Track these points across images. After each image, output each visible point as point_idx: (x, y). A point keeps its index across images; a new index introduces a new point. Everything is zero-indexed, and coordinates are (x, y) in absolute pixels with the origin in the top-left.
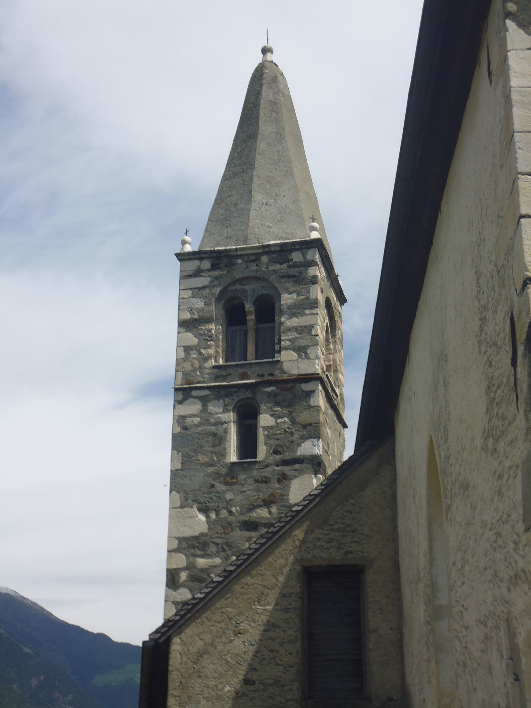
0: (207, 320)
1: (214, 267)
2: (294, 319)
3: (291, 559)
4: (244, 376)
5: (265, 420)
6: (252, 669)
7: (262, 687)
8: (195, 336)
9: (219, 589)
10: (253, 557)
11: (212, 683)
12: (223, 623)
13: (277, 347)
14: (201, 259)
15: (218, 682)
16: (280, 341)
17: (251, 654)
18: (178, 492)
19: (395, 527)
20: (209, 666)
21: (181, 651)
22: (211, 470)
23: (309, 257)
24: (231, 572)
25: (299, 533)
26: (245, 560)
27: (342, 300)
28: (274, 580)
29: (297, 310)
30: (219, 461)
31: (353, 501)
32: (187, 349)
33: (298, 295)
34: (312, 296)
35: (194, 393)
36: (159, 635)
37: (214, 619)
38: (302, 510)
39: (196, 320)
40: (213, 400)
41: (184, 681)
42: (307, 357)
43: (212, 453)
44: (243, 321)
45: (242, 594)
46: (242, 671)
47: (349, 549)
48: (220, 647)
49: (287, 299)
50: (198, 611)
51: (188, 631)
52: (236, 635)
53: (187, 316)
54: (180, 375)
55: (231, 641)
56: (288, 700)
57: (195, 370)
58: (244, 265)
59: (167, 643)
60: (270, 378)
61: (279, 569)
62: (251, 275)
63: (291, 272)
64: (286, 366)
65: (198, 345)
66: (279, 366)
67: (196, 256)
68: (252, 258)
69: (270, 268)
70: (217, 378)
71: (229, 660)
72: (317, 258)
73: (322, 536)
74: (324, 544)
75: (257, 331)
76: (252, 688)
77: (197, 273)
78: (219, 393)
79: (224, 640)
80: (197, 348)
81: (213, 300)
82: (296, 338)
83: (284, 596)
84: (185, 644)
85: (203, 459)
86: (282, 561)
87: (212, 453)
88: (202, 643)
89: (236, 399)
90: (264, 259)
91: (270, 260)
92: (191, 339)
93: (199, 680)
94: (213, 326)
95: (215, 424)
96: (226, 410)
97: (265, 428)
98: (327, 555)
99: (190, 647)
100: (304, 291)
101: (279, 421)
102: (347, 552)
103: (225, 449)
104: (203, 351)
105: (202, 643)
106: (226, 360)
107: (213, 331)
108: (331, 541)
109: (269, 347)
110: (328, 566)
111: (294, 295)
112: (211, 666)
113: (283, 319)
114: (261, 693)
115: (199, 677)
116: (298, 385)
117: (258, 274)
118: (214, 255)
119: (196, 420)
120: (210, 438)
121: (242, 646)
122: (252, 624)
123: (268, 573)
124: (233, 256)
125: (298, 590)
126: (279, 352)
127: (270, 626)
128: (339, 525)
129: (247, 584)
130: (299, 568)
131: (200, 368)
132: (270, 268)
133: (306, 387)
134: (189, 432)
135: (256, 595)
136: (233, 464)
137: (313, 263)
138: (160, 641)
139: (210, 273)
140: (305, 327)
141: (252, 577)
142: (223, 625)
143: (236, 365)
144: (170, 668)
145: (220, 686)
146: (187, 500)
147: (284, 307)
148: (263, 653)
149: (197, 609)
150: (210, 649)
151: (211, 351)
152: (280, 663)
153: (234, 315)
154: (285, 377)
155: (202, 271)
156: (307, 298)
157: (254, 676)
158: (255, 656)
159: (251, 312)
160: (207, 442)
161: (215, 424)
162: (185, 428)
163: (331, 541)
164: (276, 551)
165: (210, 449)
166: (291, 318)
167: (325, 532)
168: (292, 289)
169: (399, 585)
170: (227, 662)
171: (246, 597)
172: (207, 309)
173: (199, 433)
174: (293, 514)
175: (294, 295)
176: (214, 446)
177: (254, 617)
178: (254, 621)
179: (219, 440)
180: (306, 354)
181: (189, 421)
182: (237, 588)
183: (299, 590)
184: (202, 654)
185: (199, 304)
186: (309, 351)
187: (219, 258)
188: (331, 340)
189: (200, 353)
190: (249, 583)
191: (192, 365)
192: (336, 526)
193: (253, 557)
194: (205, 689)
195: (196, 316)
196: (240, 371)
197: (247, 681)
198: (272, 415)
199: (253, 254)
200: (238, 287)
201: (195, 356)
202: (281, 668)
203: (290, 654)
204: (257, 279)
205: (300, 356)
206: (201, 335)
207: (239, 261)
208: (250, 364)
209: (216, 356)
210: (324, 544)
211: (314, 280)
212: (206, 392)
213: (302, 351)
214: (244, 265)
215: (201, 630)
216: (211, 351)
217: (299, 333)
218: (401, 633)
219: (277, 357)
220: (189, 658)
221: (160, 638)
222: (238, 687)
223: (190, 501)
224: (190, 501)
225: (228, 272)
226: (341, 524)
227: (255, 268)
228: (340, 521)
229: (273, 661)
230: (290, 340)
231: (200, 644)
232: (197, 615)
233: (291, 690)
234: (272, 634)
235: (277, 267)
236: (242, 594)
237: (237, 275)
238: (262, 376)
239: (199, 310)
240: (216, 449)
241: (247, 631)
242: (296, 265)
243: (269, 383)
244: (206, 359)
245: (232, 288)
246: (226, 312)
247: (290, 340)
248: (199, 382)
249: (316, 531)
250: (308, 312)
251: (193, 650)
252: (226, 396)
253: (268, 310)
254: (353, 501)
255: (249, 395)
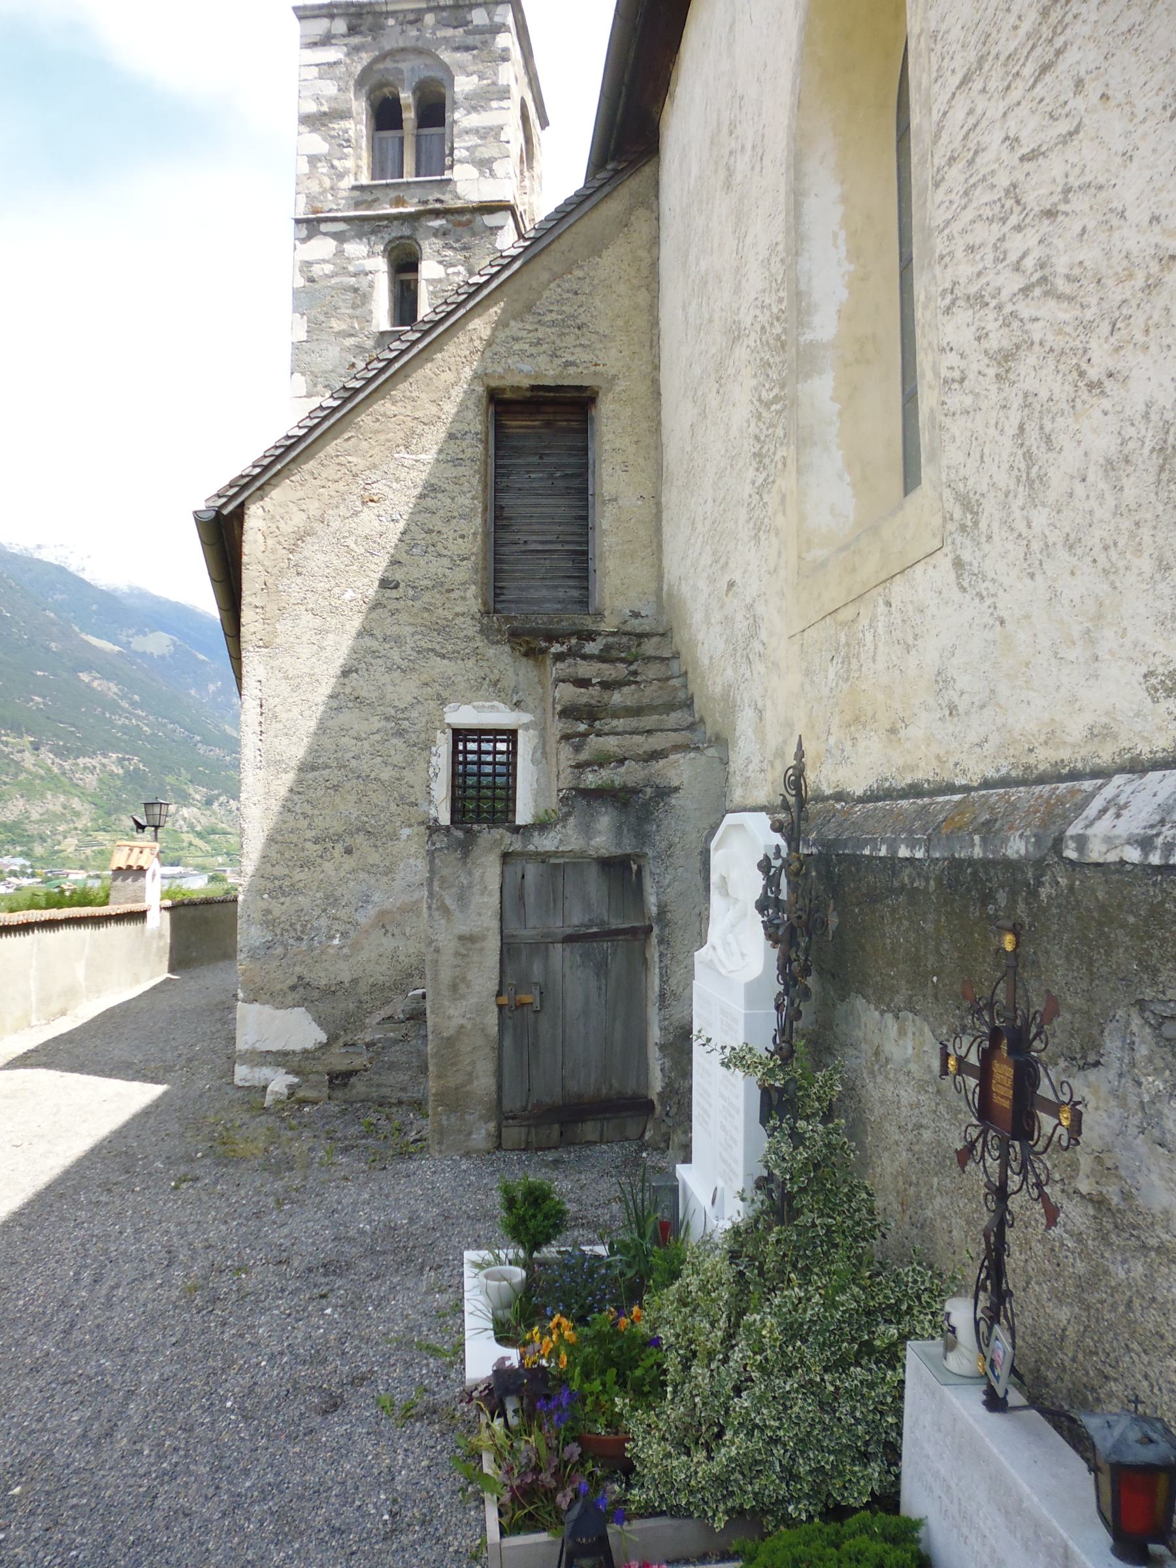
0: (344, 115)
1: (352, 30)
2: (474, 115)
3: (467, 373)
4: (399, 202)
5: (429, 270)
6: (395, 562)
7: (411, 592)
8: (325, 140)
9: (332, 421)
10: (397, 365)
11: (322, 586)
12: (341, 483)
13: (448, 161)
14: (332, 17)
15: (333, 583)
16: (452, 149)
17: (394, 538)
18: (303, 374)
19: (655, 323)
20: (315, 555)
21: (264, 529)
22: (350, 342)
23: (497, 19)
24: (357, 391)
25: (481, 326)
26: (382, 371)
27: (544, 123)
28: (434, 409)
29: (478, 101)
30: (362, 329)
31: (580, 274)
32: (313, 160)
33: (481, 78)
34: (502, 81)
35: (324, 227)
36: (224, 500)
37: (324, 475)
38: (487, 282)
39: (325, 114)
40: (353, 237)
41: (270, 581)
42: (493, 175)
43: (351, 317)
44: (397, 124)
45: (377, 432)
46: (378, 567)
47: (572, 359)
48: (336, 524)
49: (463, 85)
50: (293, 460)
51: (277, 495)
52: (364, 503)
53: (311, 107)
54: (302, 199)
55: (356, 514)
56: (457, 615)
57: (325, 191)
58: (399, 28)
59: (239, 515)
60: (438, 206)
61: (441, 397)
62: (409, 44)
63: (471, 40)
64: (461, 189)
65: (329, 154)
66: (450, 188)
67: (324, 11)
68: (411, 17)
69: (439, 34)
70: (358, 205)
71: (353, 546)
72: (510, 20)
73: (524, 334)
74: (526, 347)
75: (418, 136)
76: (394, 594)
77: (326, 40)
78: (364, 227)
79: (342, 511)
80: (327, 158)
81: (352, 83)
82: (476, 146)
83: (451, 436)
84: (273, 517)
85: (337, 325)
86: (449, 377)
87: (351, 317)
88: (304, 516)
89: (387, 238)
90: (429, 19)
91: (438, 22)
92: (317, 144)
93: (299, 580)
94: (349, 124)
95: (355, 275)
96: (371, 254)
97: (430, 281)
98: (530, 369)
99: (282, 524)
100: (489, 72)
101: (450, 270)
102: (568, 364)
103: (371, 312)
104: (336, 162)
105: (304, 516)
106: (373, 179)
107: (351, 133)
108: (539, 342)
109: (435, 160)
110: (534, 388)
111: (475, 78)
112: (320, 556)
113: (457, 116)
114: (410, 603)
115: (299, 574)
116: (478, 218)
117: (420, 44)
118: (352, 10)
119: (328, 268)
120: (350, 296)
121: (376, 523)
122: (394, 485)
123: (423, 395)
124: (381, 13)
125: (478, 427)
126: (451, 167)
127: (431, 489)
128: (554, 316)
129: (384, 415)
130: (480, 389)
131: (332, 188)
132: (439, 34)
133: (490, 220)
134: (316, 286)
135: (402, 434)
136: (383, 334)
137: (500, 28)
138: (225, 512)
139: (346, 40)
140: (491, 129)
141: (394, 403)
142: (341, 486)
143: (387, 185)
144: (245, 559)
145: (337, 590)
146: (315, 385)
147: (459, 97)
148: (418, 537)
149: (293, 454)
150: (318, 526)
151: (349, 164)
152: (445, 552)
153: (385, 115)
154: (459, 204)
155: (334, 37)
156: (494, 84)
157: (399, 575)
158: (400, 540)
159: (408, 106)
160: (344, 300)
161: (355, 275)
162: (311, 280)
163: (539, 342)
164: (439, 356)
165: (350, 311)
166: (469, 113)
167: (528, 327)
168: (471, 68)
169: (659, 423)
170: (349, 550)
171: (382, 437)
172: (342, 96)
173: (333, 288)
174: (472, 290)
175: (475, 78)
176: (354, 306)
177: (398, 474)
178: (398, 480)
179: (361, 297)
180: (491, 170)
181: (317, 270)
182: (365, 420)
183: (479, 428)
184: (302, 536)
185: (330, 88)
186: (495, 166)
187: (360, 15)
188: (526, 174)
189: (333, 167)
190: (390, 413)
191: (321, 185)
192: (548, 318)
193: (397, 365)
194: (309, 595)
195: (325, 108)
196: (393, 194)
197: (385, 584)
198: (440, 262)
199: (412, 11)
200: (389, 64)
201: (325, 170)
202: (446, 562)
203: (463, 537)
204: (418, 52)
205: (482, 174)
206: (333, 137)
207: (391, 22)
208: (408, 183)
209: (357, 167)
210: (526, 347)
211: (504, 57)
212: (342, 226)
213: (485, 165)
214: (399, 28)
215: (300, 494)
216: (349, 164)
217: (481, 138)
218: (658, 504)
219: (447, 175)
220: (279, 543)
221: (225, 505)
222: (371, 592)
223: (320, 387)
224: (320, 387)
225: (374, 39)
226: (558, 313)
227: (414, 33)
228: (555, 308)
229: (431, 549)
230: (467, 149)
231: (299, 519)
232: (292, 466)
233: (463, 598)
234: (429, 502)
235: (449, 32)
236: (377, 432)
237: (388, 44)
238: (426, 202)
239: (330, 99)
240: (358, 312)
241: (384, 498)
242: (479, 31)
243: (437, 213)
244: (341, 176)
245: (381, 66)
246: (372, 105)
247: (467, 149)
248: (330, 211)
249: (512, 323)
250: (494, 104)
251: (287, 528)
252: (373, 232)
253: (434, 111)
254: (580, 274)
255: (406, 231)
